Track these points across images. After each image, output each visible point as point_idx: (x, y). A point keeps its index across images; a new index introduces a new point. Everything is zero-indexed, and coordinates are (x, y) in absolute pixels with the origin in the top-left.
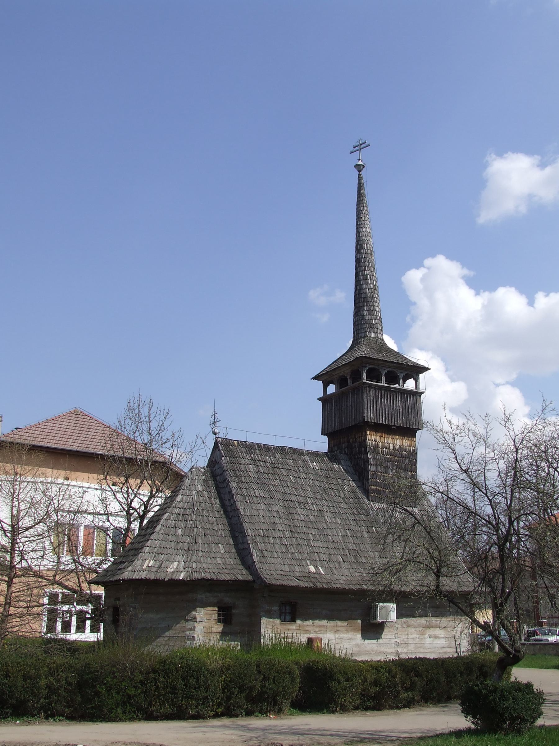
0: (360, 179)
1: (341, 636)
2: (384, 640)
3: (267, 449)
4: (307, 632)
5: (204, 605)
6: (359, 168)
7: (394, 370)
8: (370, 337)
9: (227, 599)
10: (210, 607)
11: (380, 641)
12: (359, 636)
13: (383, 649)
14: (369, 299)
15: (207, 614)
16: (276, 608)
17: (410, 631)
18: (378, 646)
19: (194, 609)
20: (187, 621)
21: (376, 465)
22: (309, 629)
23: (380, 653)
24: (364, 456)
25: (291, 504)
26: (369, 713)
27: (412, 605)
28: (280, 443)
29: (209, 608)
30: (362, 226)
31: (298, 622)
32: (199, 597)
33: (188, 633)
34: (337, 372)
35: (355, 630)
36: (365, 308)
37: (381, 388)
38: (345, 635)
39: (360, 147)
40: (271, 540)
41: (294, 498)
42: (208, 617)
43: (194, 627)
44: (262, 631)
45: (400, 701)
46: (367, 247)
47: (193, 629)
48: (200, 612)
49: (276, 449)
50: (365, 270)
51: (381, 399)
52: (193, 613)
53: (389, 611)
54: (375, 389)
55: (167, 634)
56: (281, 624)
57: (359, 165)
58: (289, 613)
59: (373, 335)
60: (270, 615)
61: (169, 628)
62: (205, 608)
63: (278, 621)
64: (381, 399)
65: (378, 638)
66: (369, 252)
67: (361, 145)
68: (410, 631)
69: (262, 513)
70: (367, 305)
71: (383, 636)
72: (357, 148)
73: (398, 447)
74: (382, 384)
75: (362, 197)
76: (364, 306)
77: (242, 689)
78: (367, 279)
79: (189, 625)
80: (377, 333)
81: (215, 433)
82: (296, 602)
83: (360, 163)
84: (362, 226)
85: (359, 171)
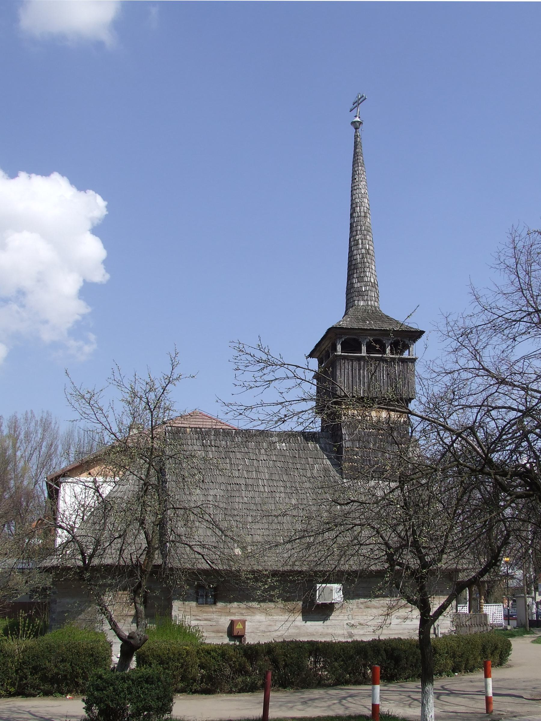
0: (356, 137)
1: (274, 617)
2: (333, 621)
4: (229, 613)
6: (356, 125)
7: (378, 338)
8: (358, 305)
11: (327, 623)
12: (300, 618)
13: (330, 631)
14: (360, 265)
17: (370, 612)
18: (325, 627)
21: (352, 441)
23: (327, 634)
24: (339, 433)
25: (236, 487)
26: (196, 696)
27: (360, 585)
30: (356, 188)
31: (220, 605)
34: (323, 347)
35: (292, 611)
36: (355, 276)
37: (359, 359)
38: (281, 617)
39: (357, 103)
41: (242, 481)
44: (173, 613)
45: (236, 686)
46: (360, 209)
49: (238, 432)
50: (357, 235)
51: (359, 370)
53: (334, 592)
54: (352, 360)
56: (197, 606)
57: (355, 122)
59: (362, 303)
63: (194, 604)
64: (359, 370)
65: (324, 620)
66: (363, 214)
67: (359, 100)
68: (370, 612)
70: (357, 272)
71: (331, 618)
72: (356, 105)
73: (375, 419)
74: (363, 354)
75: (357, 156)
76: (354, 274)
77: (35, 670)
78: (358, 244)
80: (367, 300)
82: (217, 586)
83: (357, 119)
84: (356, 188)
85: (356, 129)
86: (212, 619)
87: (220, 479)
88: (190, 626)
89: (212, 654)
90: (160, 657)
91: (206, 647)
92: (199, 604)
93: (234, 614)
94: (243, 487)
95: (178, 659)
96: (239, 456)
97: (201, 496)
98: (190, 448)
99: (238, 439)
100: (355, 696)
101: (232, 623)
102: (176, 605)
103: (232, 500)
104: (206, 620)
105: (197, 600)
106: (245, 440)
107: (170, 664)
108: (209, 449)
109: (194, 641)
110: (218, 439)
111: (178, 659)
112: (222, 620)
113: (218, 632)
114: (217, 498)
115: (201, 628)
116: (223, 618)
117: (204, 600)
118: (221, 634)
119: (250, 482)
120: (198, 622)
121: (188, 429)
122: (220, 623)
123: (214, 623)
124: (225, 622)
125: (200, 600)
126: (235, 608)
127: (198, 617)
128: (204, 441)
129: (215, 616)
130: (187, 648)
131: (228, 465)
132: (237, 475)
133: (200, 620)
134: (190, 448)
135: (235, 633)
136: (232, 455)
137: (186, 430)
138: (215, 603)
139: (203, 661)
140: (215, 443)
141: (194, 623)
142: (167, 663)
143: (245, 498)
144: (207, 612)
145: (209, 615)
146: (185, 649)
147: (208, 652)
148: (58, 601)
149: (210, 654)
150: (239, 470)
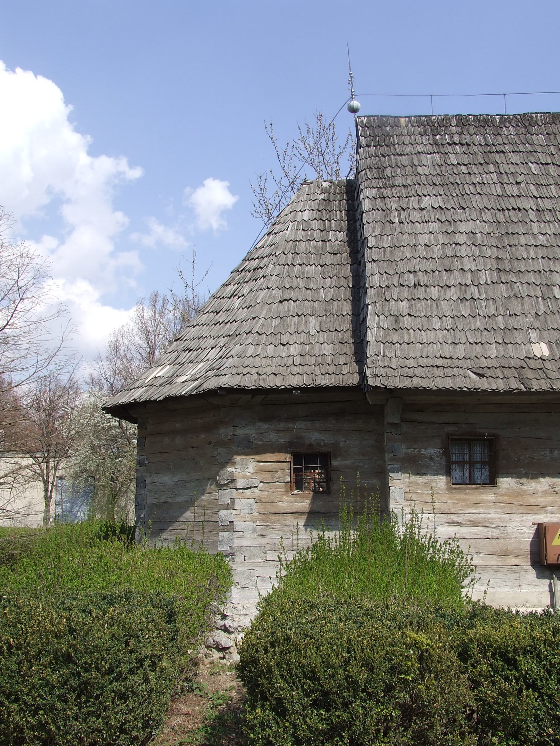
3: (483, 122)
4: (532, 508)
5: (253, 448)
9: (316, 436)
10: (273, 452)
15: (260, 471)
16: (433, 451)
19: (229, 461)
20: (221, 486)
22: (541, 500)
25: (514, 216)
28: (516, 107)
29: (269, 457)
31: (506, 483)
32: (240, 432)
33: (222, 513)
40: (434, 292)
41: (528, 204)
42: (267, 477)
43: (233, 500)
47: (230, 506)
48: (245, 466)
49: (505, 120)
52: (230, 469)
55: (188, 515)
56: (449, 489)
58: (482, 463)
60: (415, 466)
61: (190, 503)
62: (257, 457)
63: (441, 481)
69: (425, 239)
79: (224, 496)
81: (353, 110)
86: (490, 521)
87: (478, 202)
88: (433, 544)
89: (524, 667)
90: (314, 678)
91: (499, 635)
92: (455, 484)
93: (542, 508)
94: (533, 215)
95: (389, 689)
96: (514, 158)
97: (440, 235)
98: (408, 149)
99: (509, 131)
100: (452, 522)
101: (541, 532)
102: (399, 483)
103: (513, 240)
104: (474, 523)
105: (448, 473)
106: (523, 130)
107: (357, 705)
108: (449, 149)
109: (446, 603)
110: (465, 132)
111: (389, 689)
112: (513, 525)
113: (506, 554)
114: (475, 238)
115: (464, 546)
116: (516, 518)
117: (467, 474)
118: (514, 561)
119: (547, 204)
120: (457, 528)
121: (402, 120)
122: (510, 530)
123: (495, 533)
124: (522, 529)
125: (457, 473)
126: (544, 493)
127: (454, 518)
128: (438, 137)
129: (493, 514)
130: (422, 638)
131: (494, 176)
132: (516, 192)
133: (460, 524)
134: (408, 149)
135: (552, 558)
136: (498, 158)
137: (399, 121)
138: (492, 481)
139: (491, 694)
140: (461, 139)
141: (444, 532)
142: (346, 705)
143: (541, 237)
144: (474, 504)
145: (481, 510)
146: (415, 645)
147: (507, 658)
148: (148, 480)
149: (512, 663)
150: (518, 183)
